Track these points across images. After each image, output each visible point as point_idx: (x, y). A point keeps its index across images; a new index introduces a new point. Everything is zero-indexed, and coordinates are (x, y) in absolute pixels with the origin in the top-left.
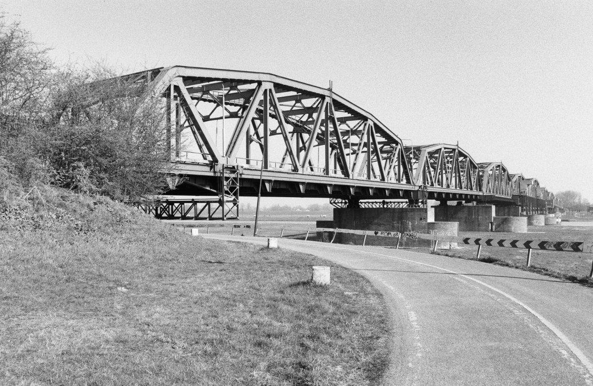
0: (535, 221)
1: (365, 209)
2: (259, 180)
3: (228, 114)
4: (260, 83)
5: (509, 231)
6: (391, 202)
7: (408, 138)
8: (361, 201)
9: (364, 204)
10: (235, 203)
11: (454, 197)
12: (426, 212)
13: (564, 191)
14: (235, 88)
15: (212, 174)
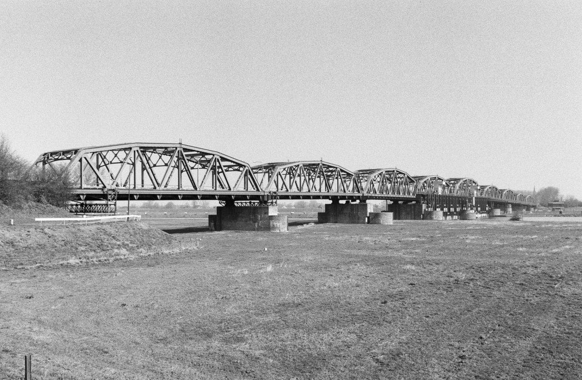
0: (434, 216)
1: (240, 207)
2: (128, 195)
3: (119, 162)
4: (176, 148)
5: (379, 223)
6: (97, 205)
7: (352, 169)
8: (236, 202)
9: (238, 203)
10: (115, 205)
11: (343, 198)
12: (268, 209)
13: (546, 186)
14: (203, 156)
15: (102, 193)
